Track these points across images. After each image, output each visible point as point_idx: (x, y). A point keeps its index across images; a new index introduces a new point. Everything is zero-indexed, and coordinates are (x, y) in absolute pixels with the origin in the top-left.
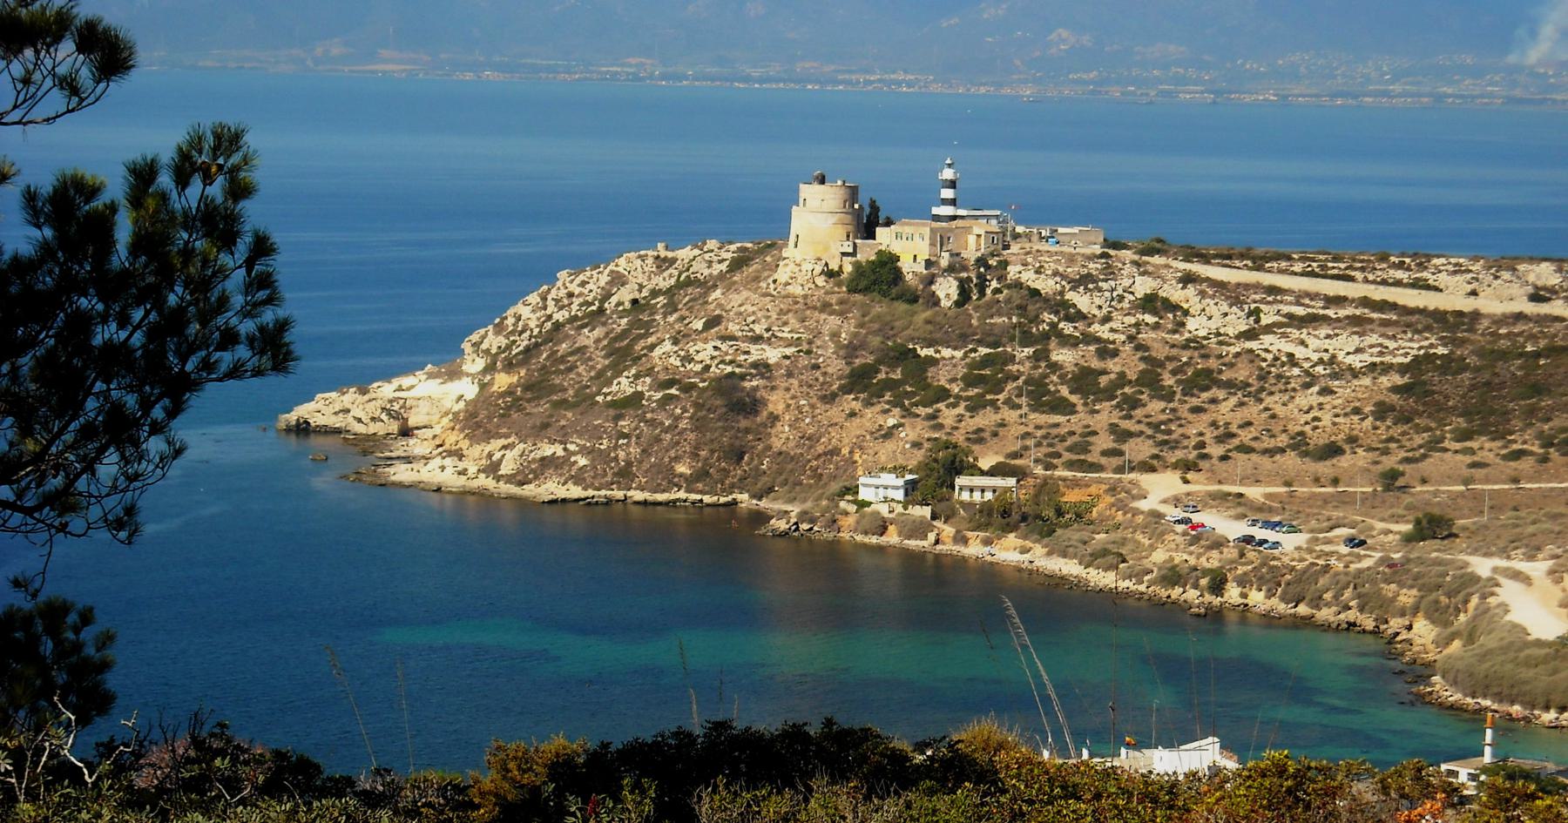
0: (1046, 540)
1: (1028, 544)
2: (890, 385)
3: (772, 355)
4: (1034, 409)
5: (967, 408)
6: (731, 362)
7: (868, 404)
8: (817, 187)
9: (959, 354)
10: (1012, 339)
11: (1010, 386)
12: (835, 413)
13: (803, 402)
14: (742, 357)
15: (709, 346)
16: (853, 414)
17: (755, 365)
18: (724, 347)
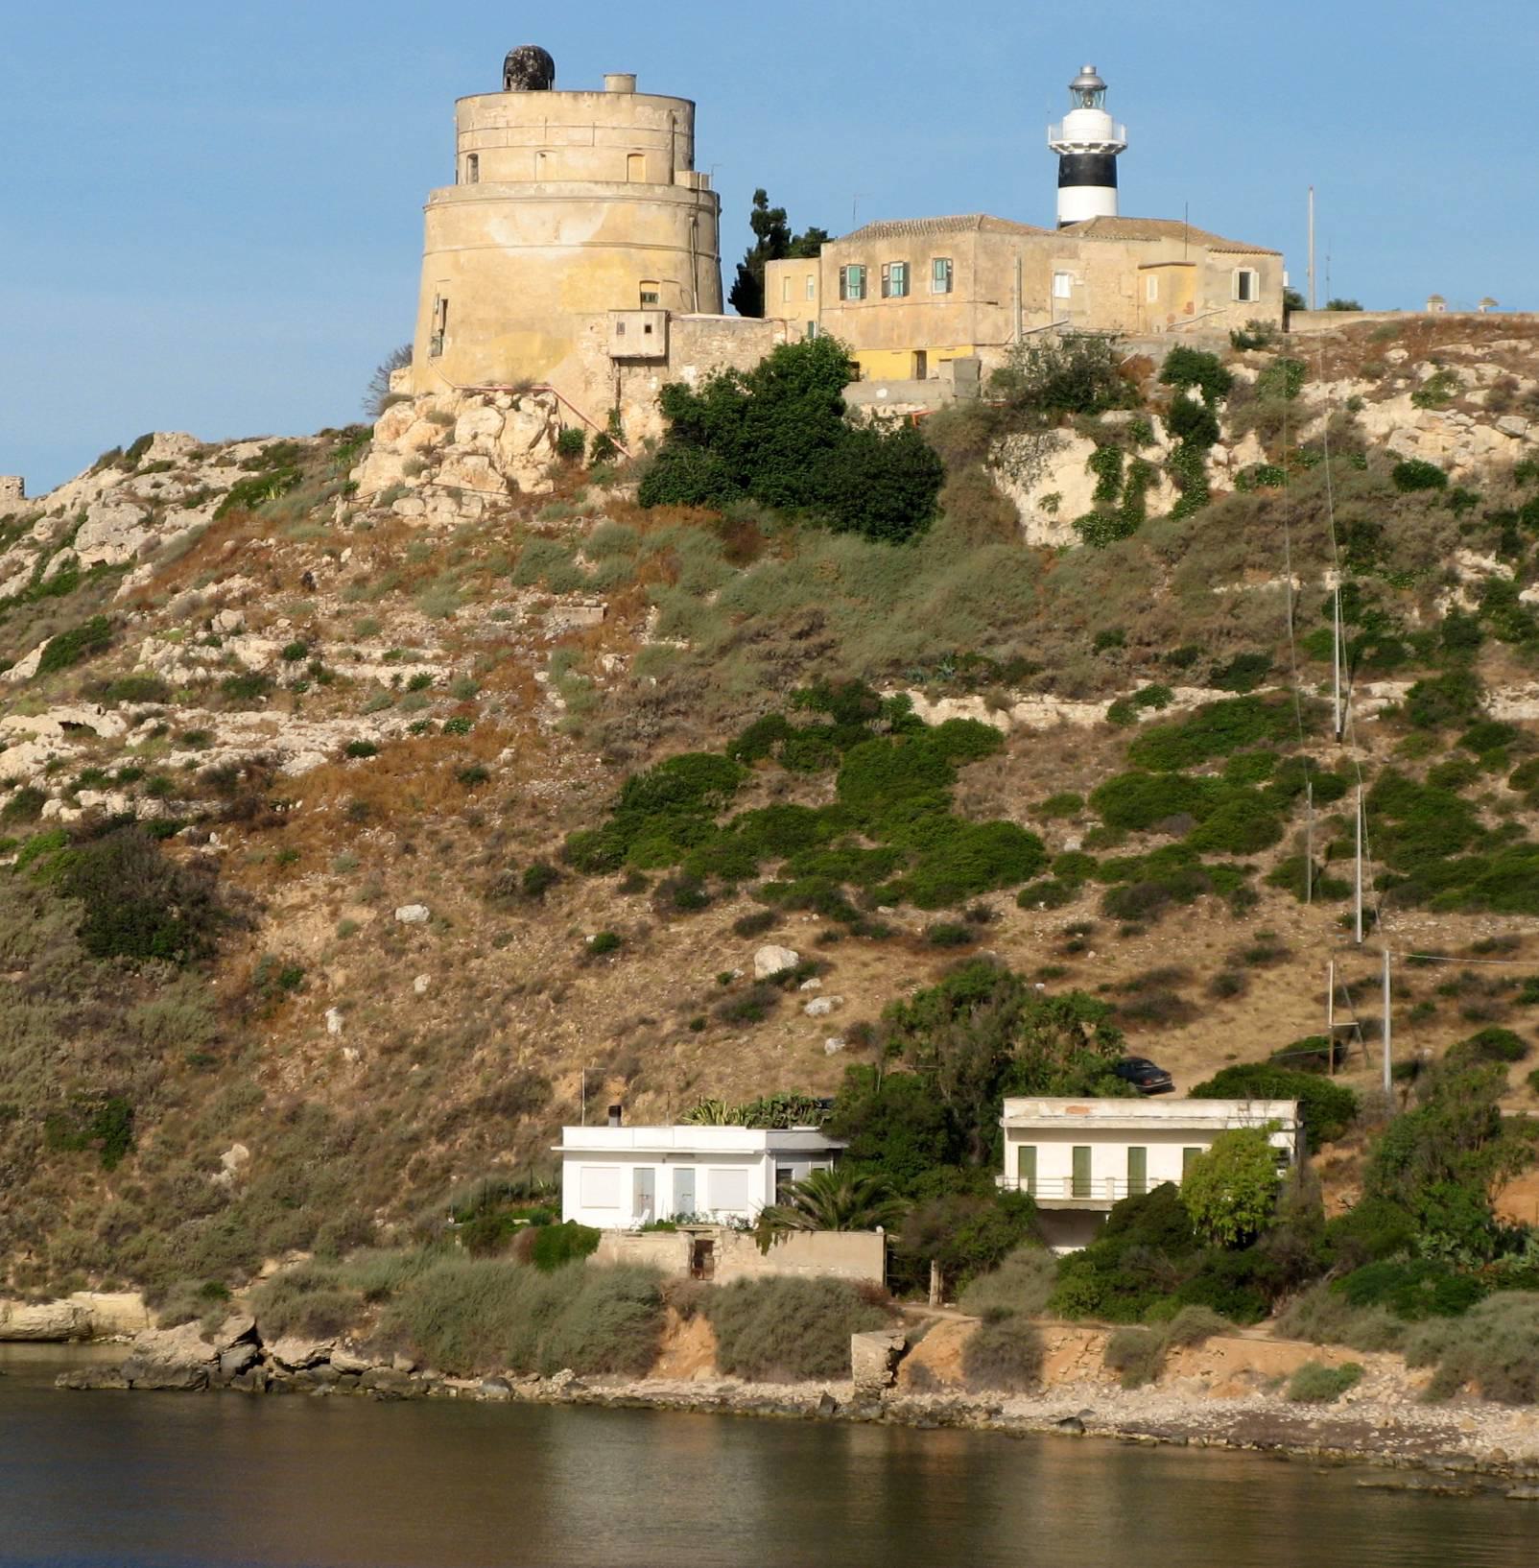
0: (1431, 1329)
1: (1337, 1357)
2: (786, 831)
3: (306, 744)
4: (1398, 892)
5: (1114, 906)
6: (129, 776)
7: (686, 901)
8: (524, 104)
9: (1089, 714)
10: (1319, 648)
11: (1307, 821)
12: (534, 946)
13: (410, 912)
14: (178, 758)
15: (48, 724)
16: (609, 945)
17: (221, 781)
18: (108, 725)
